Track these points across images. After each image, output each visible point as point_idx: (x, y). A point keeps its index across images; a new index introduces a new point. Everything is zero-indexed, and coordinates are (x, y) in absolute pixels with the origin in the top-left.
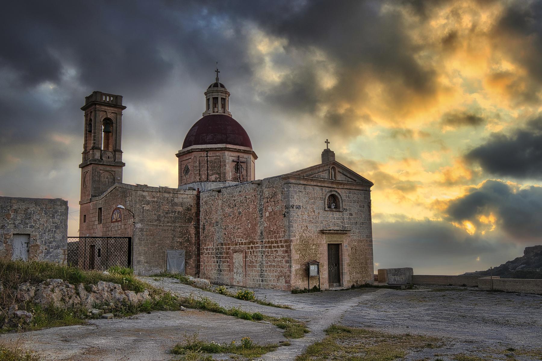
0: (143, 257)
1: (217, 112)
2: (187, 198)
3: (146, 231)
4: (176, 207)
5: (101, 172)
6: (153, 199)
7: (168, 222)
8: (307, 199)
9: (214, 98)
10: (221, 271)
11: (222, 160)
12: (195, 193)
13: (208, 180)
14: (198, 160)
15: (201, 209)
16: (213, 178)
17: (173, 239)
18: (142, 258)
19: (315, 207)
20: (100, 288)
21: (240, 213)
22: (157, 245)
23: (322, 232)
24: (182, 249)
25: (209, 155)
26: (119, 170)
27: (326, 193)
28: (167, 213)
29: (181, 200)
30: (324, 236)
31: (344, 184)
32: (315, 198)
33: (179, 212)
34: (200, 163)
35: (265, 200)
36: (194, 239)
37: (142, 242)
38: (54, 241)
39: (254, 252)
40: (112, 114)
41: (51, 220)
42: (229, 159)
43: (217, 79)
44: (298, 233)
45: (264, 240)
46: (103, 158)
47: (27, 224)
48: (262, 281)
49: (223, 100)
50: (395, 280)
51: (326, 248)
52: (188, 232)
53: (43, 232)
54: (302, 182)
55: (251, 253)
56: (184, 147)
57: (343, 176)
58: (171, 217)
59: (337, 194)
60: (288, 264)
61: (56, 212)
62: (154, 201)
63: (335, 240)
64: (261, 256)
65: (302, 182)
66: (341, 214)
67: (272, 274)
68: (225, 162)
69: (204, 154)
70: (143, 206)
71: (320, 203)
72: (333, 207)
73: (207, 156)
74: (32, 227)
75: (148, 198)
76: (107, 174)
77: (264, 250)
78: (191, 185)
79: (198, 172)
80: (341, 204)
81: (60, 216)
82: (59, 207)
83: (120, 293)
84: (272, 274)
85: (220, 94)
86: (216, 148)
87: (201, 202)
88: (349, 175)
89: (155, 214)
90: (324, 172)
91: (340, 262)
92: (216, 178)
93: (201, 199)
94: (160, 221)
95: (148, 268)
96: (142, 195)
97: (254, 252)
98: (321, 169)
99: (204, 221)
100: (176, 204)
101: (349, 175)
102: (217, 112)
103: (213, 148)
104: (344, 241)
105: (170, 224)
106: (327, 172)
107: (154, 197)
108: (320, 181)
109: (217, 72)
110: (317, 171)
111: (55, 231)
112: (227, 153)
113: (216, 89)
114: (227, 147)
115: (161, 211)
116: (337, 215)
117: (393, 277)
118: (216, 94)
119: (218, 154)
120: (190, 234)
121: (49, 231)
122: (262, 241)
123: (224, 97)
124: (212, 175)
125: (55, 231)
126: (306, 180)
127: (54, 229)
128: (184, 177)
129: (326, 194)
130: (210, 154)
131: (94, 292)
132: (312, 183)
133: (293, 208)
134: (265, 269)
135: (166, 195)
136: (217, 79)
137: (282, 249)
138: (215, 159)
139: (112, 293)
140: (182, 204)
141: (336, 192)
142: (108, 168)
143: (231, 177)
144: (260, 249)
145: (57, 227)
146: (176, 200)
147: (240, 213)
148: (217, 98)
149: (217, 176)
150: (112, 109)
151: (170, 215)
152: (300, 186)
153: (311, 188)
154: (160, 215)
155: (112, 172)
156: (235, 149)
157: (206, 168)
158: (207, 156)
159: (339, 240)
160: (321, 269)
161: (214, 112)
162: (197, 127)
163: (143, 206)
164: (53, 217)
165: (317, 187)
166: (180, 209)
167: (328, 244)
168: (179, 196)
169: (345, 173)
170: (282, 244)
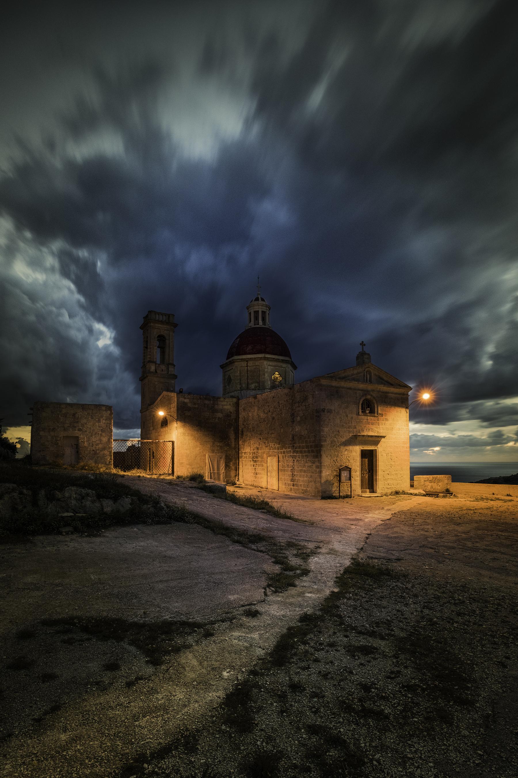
1: (258, 324)
6: (194, 406)
9: (255, 312)
10: (256, 474)
11: (261, 369)
12: (235, 400)
13: (248, 388)
15: (240, 416)
16: (253, 386)
20: (67, 495)
21: (273, 418)
25: (249, 365)
33: (219, 418)
34: (240, 373)
35: (297, 405)
38: (101, 443)
39: (286, 456)
41: (97, 424)
42: (268, 368)
45: (295, 445)
46: (158, 371)
47: (76, 427)
48: (293, 485)
50: (432, 487)
53: (90, 434)
55: (283, 458)
56: (227, 359)
60: (318, 470)
61: (102, 417)
64: (292, 461)
67: (302, 479)
72: (368, 412)
73: (247, 366)
74: (80, 430)
75: (189, 405)
77: (295, 454)
78: (233, 394)
79: (239, 381)
80: (376, 409)
81: (106, 420)
82: (104, 412)
83: (93, 502)
84: (302, 479)
86: (255, 358)
87: (240, 408)
91: (374, 468)
92: (256, 387)
93: (240, 406)
97: (286, 456)
99: (243, 426)
102: (258, 324)
103: (252, 358)
107: (195, 404)
111: (101, 435)
113: (256, 302)
114: (266, 356)
117: (430, 484)
118: (257, 307)
119: (257, 363)
121: (95, 434)
122: (294, 446)
123: (265, 310)
124: (252, 383)
125: (101, 435)
127: (100, 433)
128: (228, 387)
130: (250, 363)
131: (59, 500)
133: (324, 411)
134: (295, 473)
137: (313, 454)
139: (83, 501)
143: (269, 386)
144: (292, 454)
145: (102, 431)
147: (273, 418)
149: (257, 385)
157: (246, 377)
158: (247, 366)
160: (353, 473)
162: (238, 339)
164: (99, 421)
170: (313, 449)
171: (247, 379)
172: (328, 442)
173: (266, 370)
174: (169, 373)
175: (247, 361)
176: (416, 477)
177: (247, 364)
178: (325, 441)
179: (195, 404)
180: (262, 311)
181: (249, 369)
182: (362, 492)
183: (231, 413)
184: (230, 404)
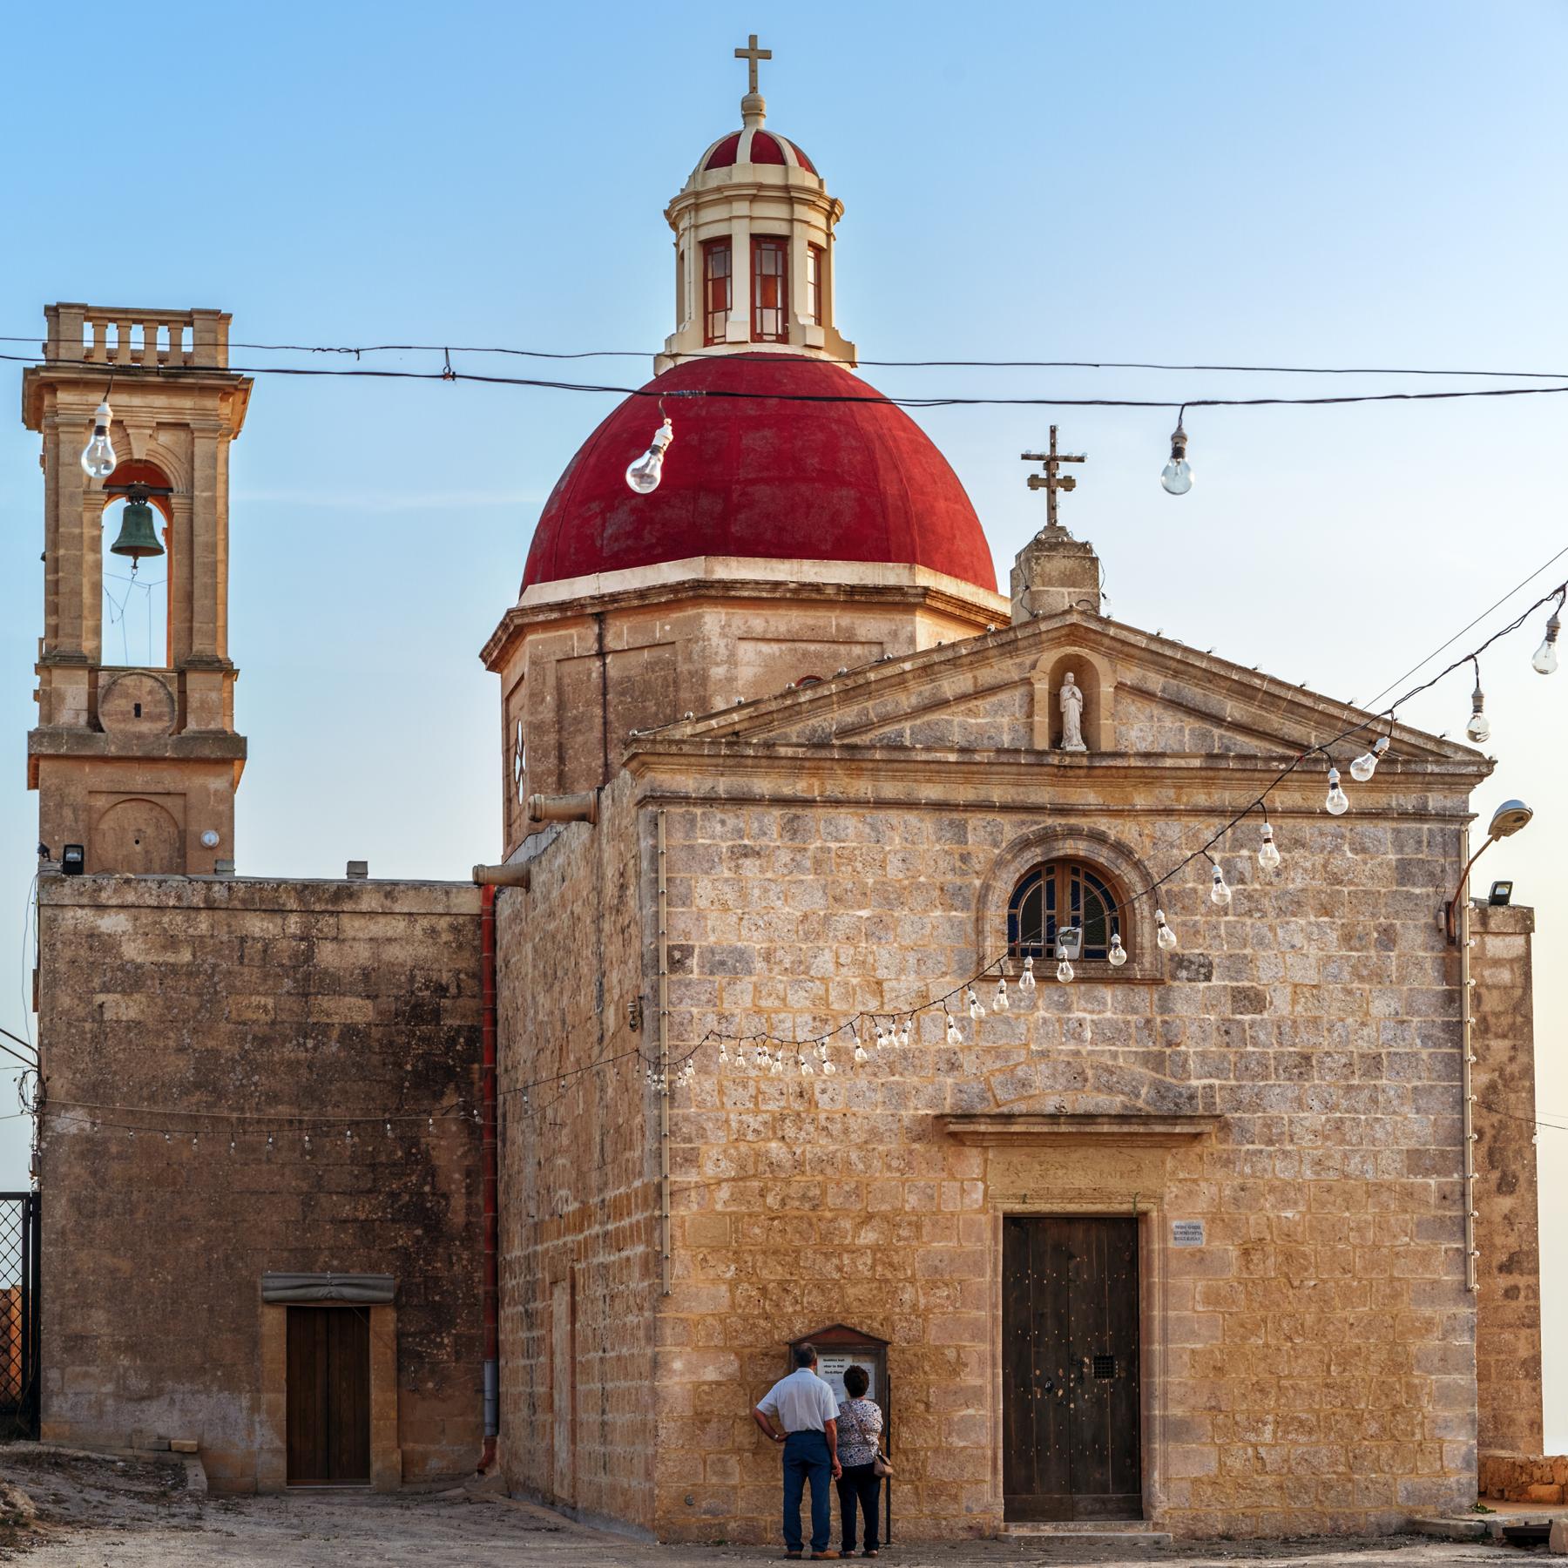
0: (99, 1316)
1: (783, 338)
2: (408, 940)
3: (120, 1157)
4: (326, 1002)
5: (101, 802)
6: (170, 957)
7: (273, 1098)
8: (817, 903)
9: (757, 240)
11: (683, 668)
14: (551, 681)
17: (308, 1201)
18: (98, 1321)
19: (884, 956)
22: (195, 1243)
23: (953, 1130)
24: (374, 1267)
25: (611, 643)
26: (216, 783)
27: (994, 851)
28: (263, 1041)
29: (363, 954)
30: (972, 1161)
31: (1181, 778)
32: (891, 897)
33: (350, 1032)
34: (561, 706)
36: (459, 1201)
37: (100, 1225)
40: (165, 437)
42: (732, 660)
43: (751, 109)
44: (719, 1137)
49: (774, 246)
51: (989, 1245)
52: (417, 1157)
54: (763, 785)
57: (1170, 720)
58: (292, 1066)
59: (1103, 857)
62: (173, 969)
63: (1078, 1184)
65: (763, 785)
66: (1144, 998)
68: (704, 679)
69: (581, 638)
70: (100, 998)
71: (933, 924)
73: (601, 654)
75: (132, 951)
76: (135, 816)
85: (741, 208)
86: (642, 594)
88: (1233, 709)
89: (181, 1050)
90: (983, 704)
94: (220, 1094)
95: (139, 1384)
96: (93, 935)
98: (953, 684)
100: (332, 984)
101: (1233, 709)
103: (817, 588)
104: (1172, 1190)
105: (284, 1110)
106: (1016, 696)
107: (172, 943)
108: (937, 770)
109: (753, 53)
110: (907, 700)
112: (713, 620)
115: (224, 1027)
116: (1109, 1004)
119: (662, 627)
120: (431, 1172)
123: (780, 229)
126: (797, 766)
129: (999, 863)
130: (621, 633)
132: (863, 787)
135: (257, 925)
136: (751, 109)
138: (650, 666)
140: (368, 981)
141: (1098, 838)
142: (140, 779)
146: (327, 955)
148: (725, 242)
150: (160, 401)
151: (289, 1051)
152: (749, 819)
153: (848, 821)
154: (215, 1053)
155: (168, 802)
156: (776, 585)
157: (597, 733)
158: (601, 654)
159: (1115, 1183)
161: (757, 337)
163: (100, 998)
165: (912, 818)
166: (354, 1010)
167: (1011, 1220)
168: (352, 926)
169: (1193, 693)
171: (605, 743)
172: (710, 1170)
173: (718, 672)
174: (192, 725)
175: (600, 618)
176: (18, 1205)
177: (600, 638)
178: (691, 1159)
179: (172, 943)
180: (757, 240)
181: (613, 673)
182: (1012, 1514)
183: (441, 990)
184: (433, 932)
